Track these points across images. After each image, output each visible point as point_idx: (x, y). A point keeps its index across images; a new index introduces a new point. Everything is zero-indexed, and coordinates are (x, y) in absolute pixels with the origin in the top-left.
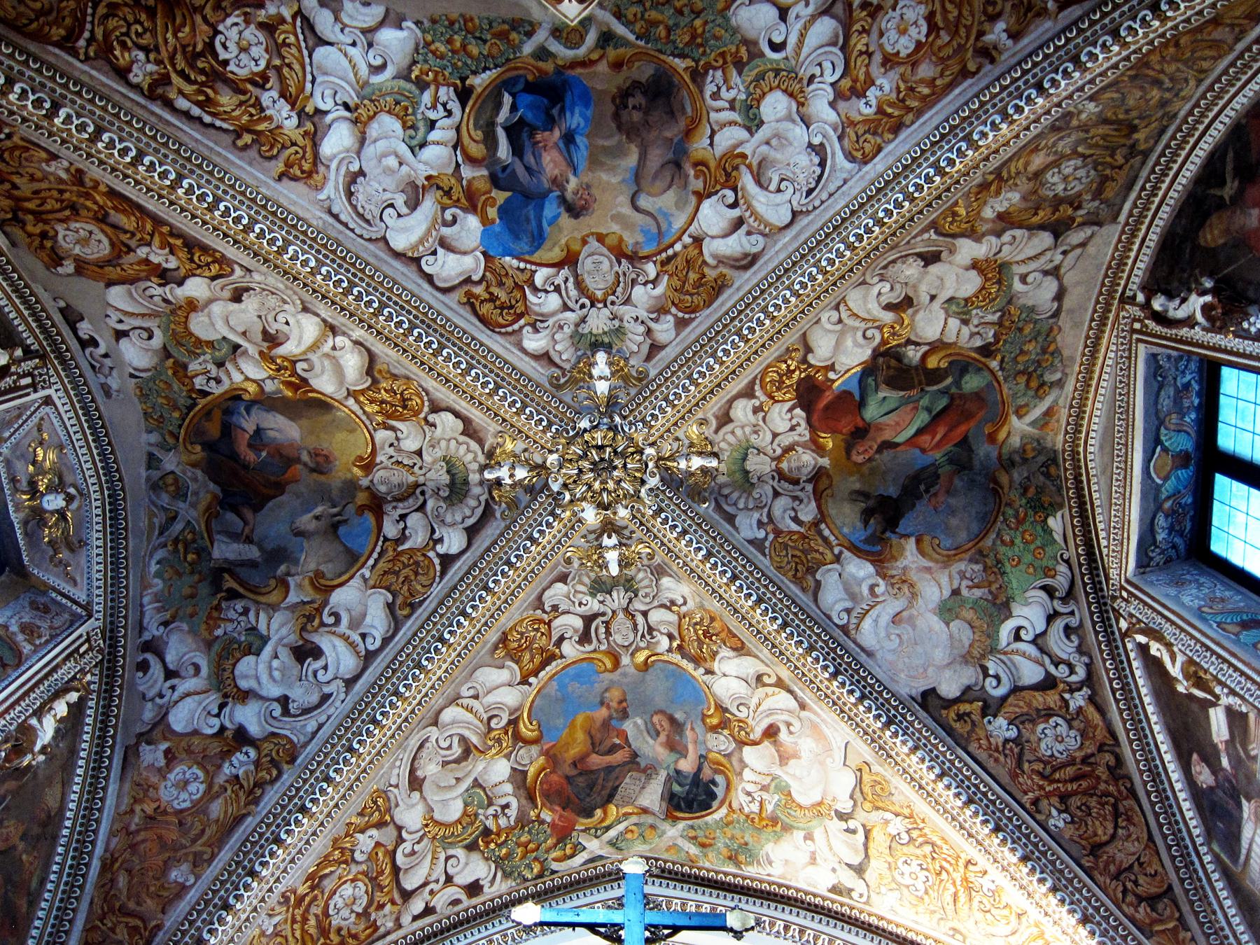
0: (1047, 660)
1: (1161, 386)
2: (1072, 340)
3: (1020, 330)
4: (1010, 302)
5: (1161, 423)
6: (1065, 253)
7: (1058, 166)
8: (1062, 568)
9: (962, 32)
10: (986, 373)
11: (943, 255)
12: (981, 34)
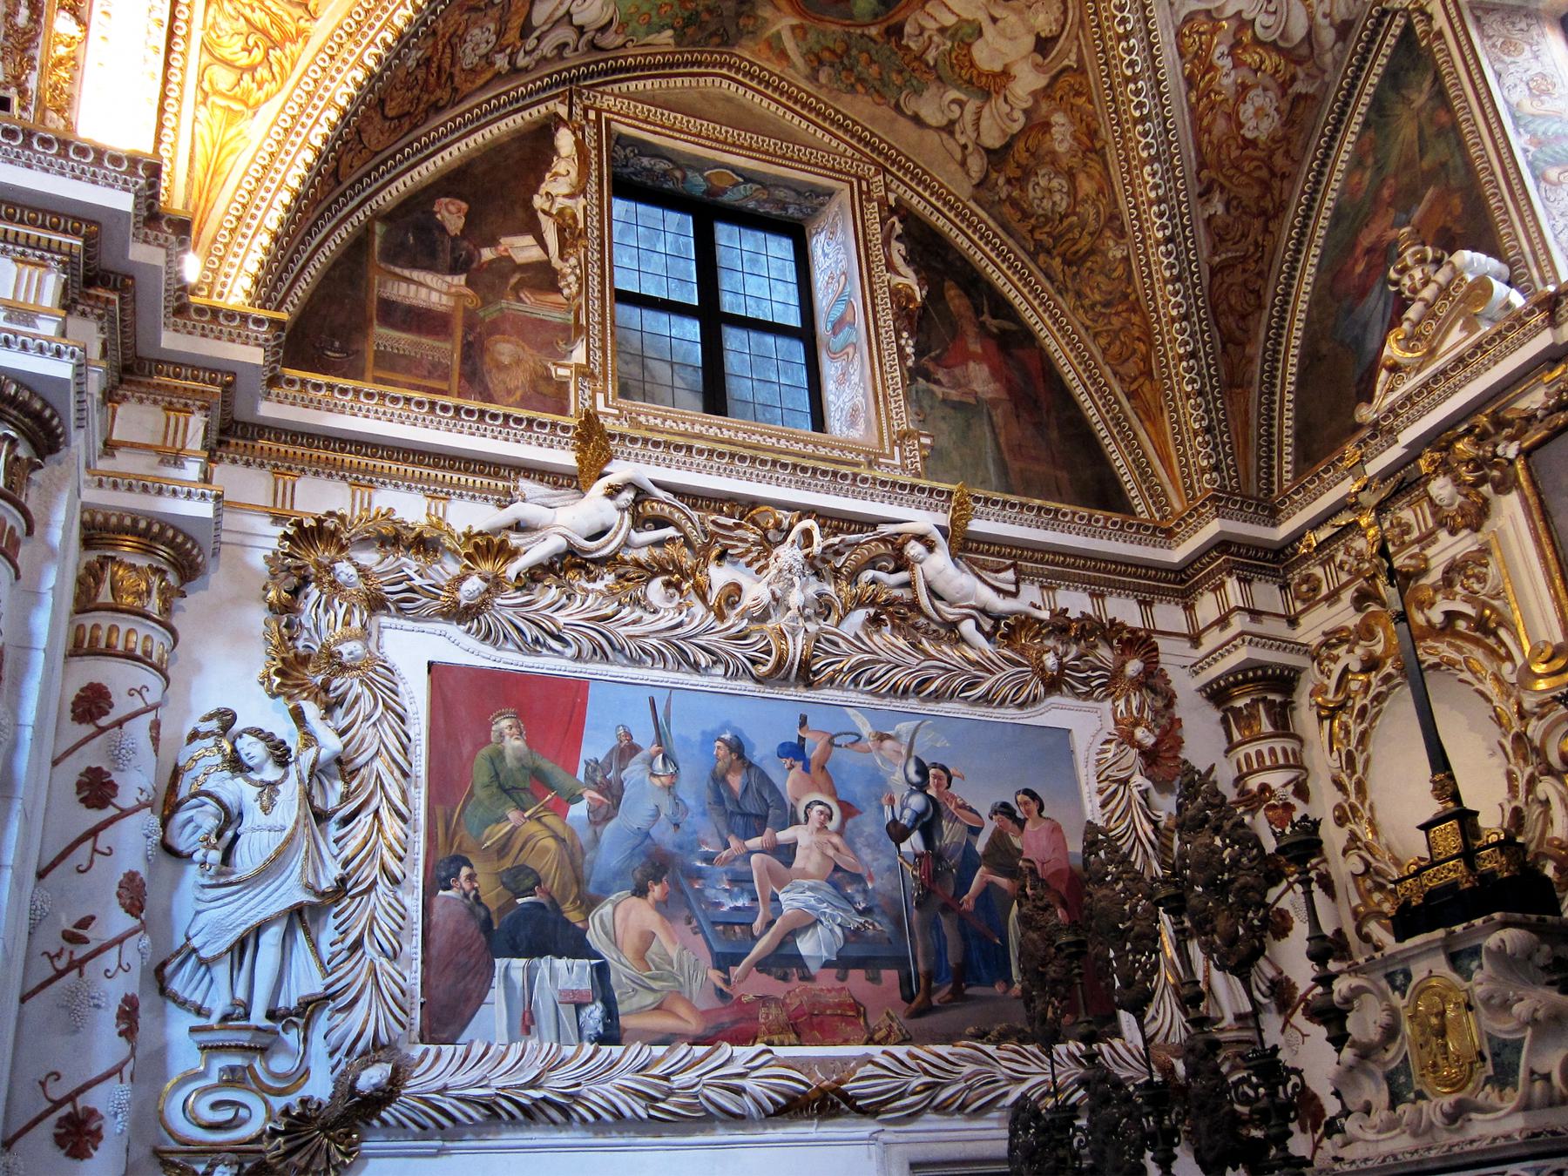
0: (545, 28)
1: (799, 193)
2: (860, 108)
3: (900, 72)
4: (939, 78)
5: (764, 187)
6: (965, 147)
7: (1068, 194)
8: (620, 40)
9: (1232, 172)
10: (867, 20)
11: (1039, 59)
12: (1222, 188)
